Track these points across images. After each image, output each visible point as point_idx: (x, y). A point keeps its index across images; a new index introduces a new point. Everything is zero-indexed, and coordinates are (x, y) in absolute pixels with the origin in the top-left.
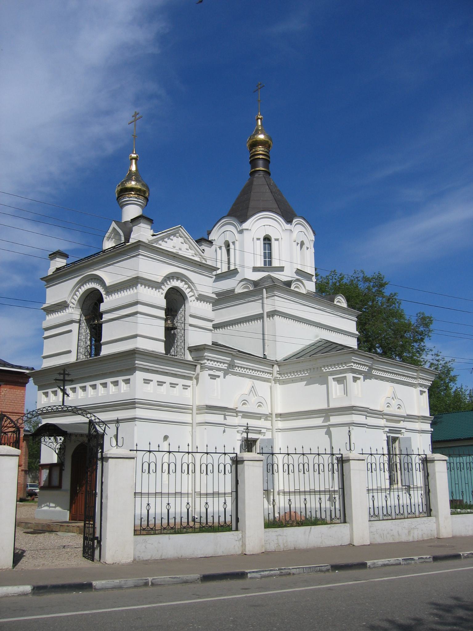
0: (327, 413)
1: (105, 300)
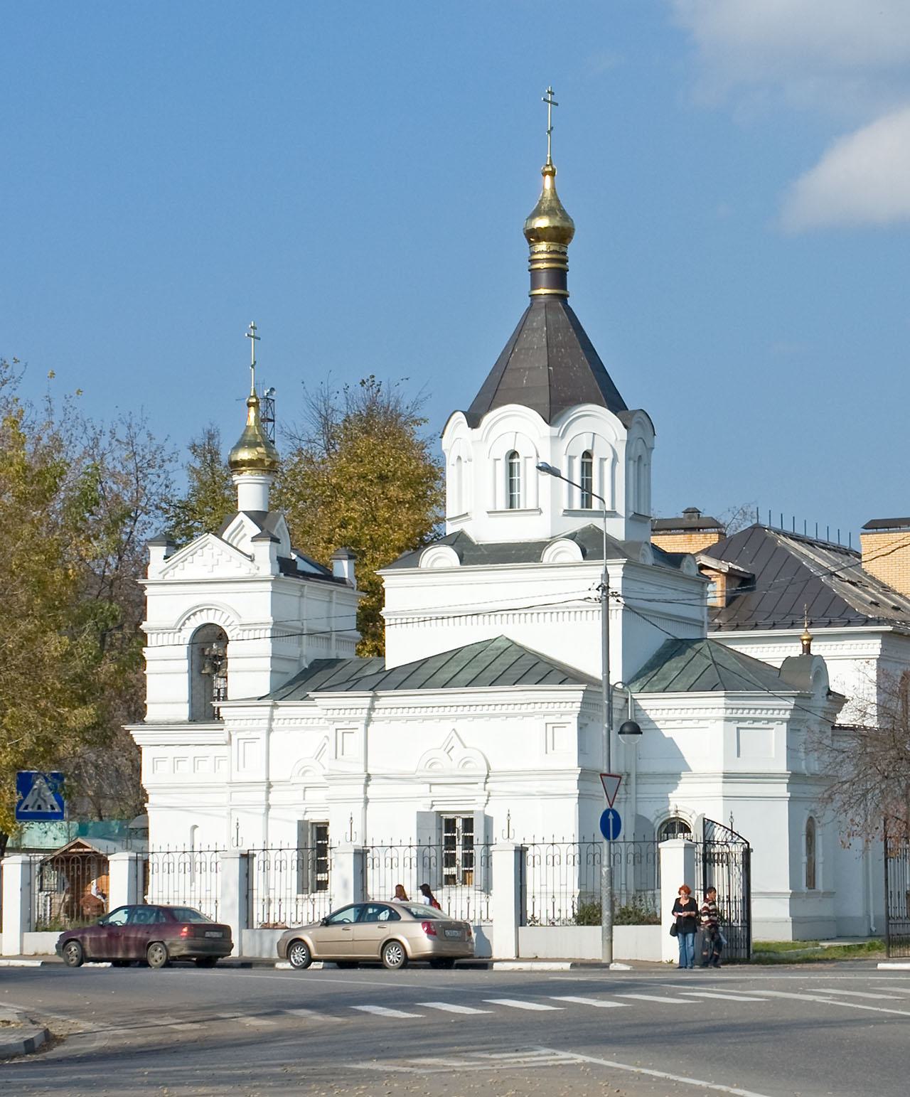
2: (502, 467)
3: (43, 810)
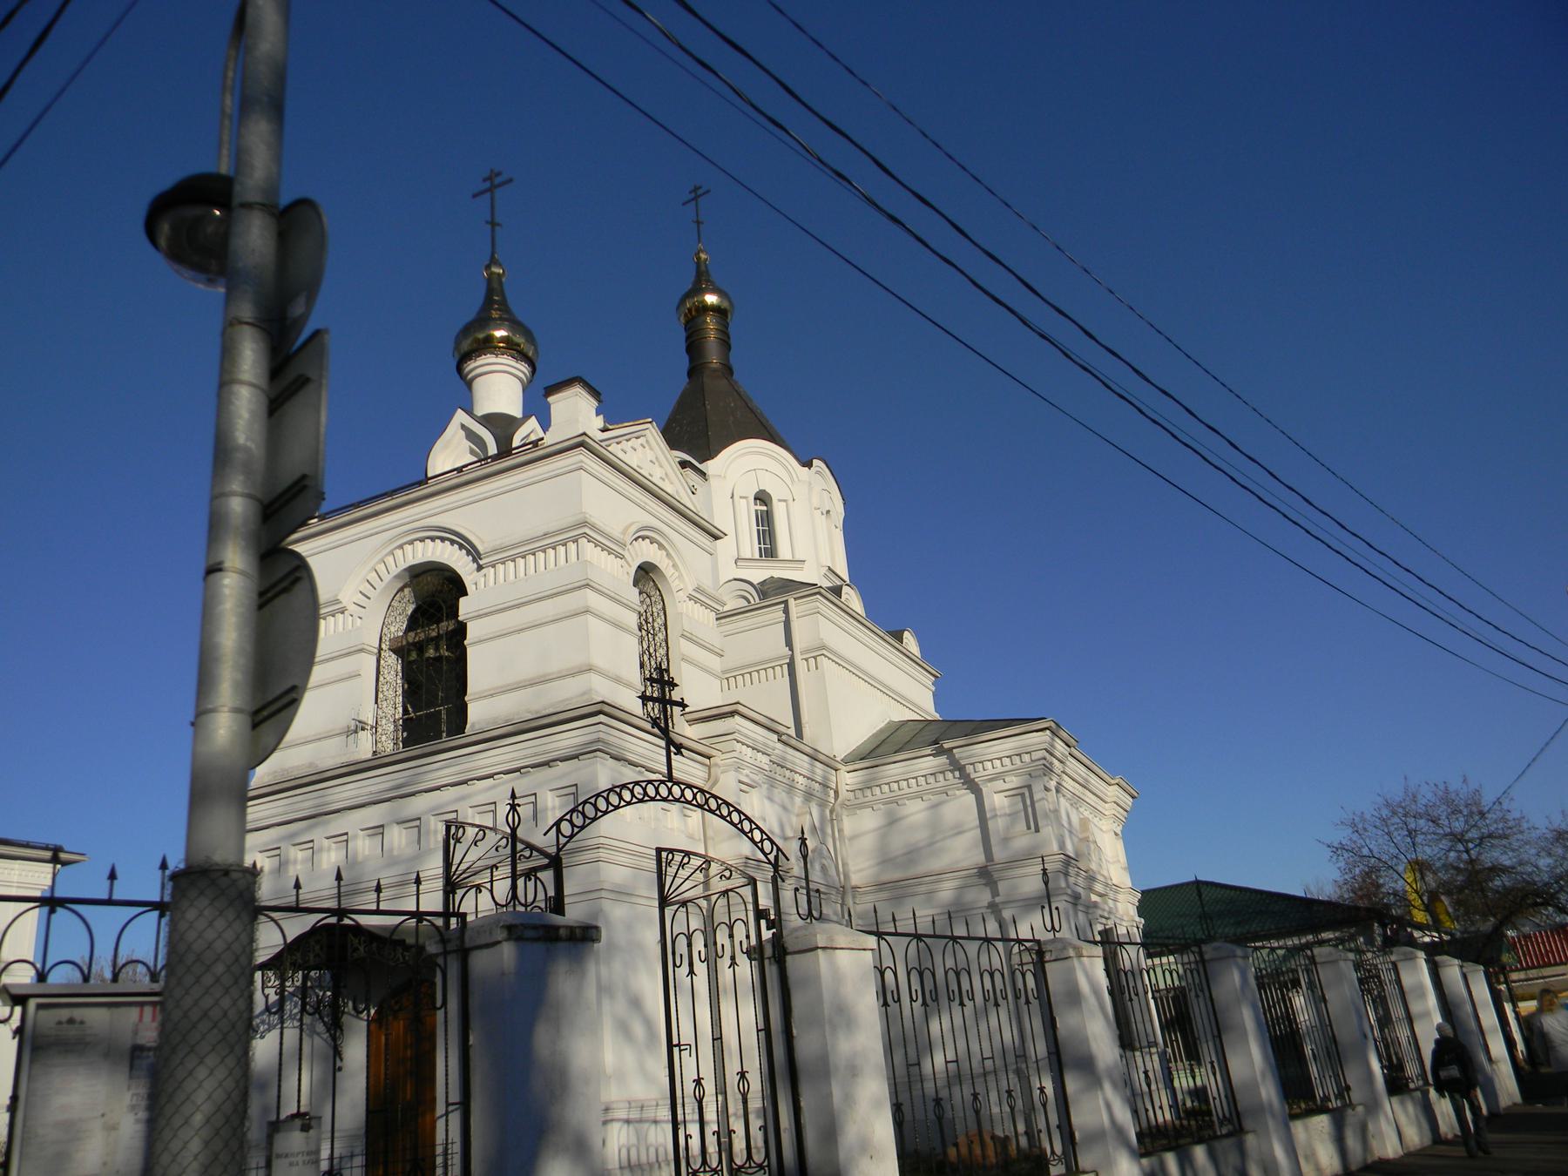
1: (470, 587)
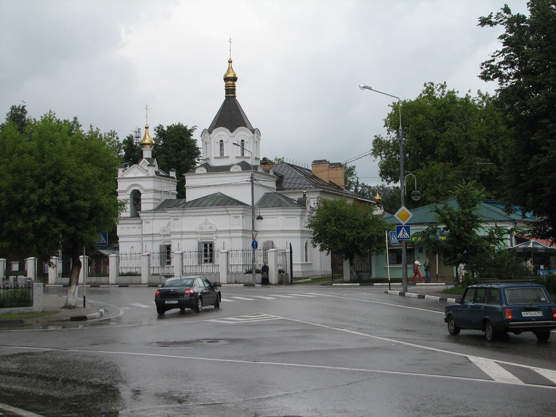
0: (230, 231)
2: (218, 146)
3: (101, 242)
